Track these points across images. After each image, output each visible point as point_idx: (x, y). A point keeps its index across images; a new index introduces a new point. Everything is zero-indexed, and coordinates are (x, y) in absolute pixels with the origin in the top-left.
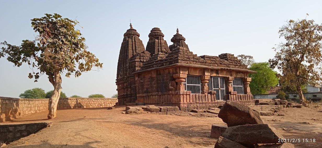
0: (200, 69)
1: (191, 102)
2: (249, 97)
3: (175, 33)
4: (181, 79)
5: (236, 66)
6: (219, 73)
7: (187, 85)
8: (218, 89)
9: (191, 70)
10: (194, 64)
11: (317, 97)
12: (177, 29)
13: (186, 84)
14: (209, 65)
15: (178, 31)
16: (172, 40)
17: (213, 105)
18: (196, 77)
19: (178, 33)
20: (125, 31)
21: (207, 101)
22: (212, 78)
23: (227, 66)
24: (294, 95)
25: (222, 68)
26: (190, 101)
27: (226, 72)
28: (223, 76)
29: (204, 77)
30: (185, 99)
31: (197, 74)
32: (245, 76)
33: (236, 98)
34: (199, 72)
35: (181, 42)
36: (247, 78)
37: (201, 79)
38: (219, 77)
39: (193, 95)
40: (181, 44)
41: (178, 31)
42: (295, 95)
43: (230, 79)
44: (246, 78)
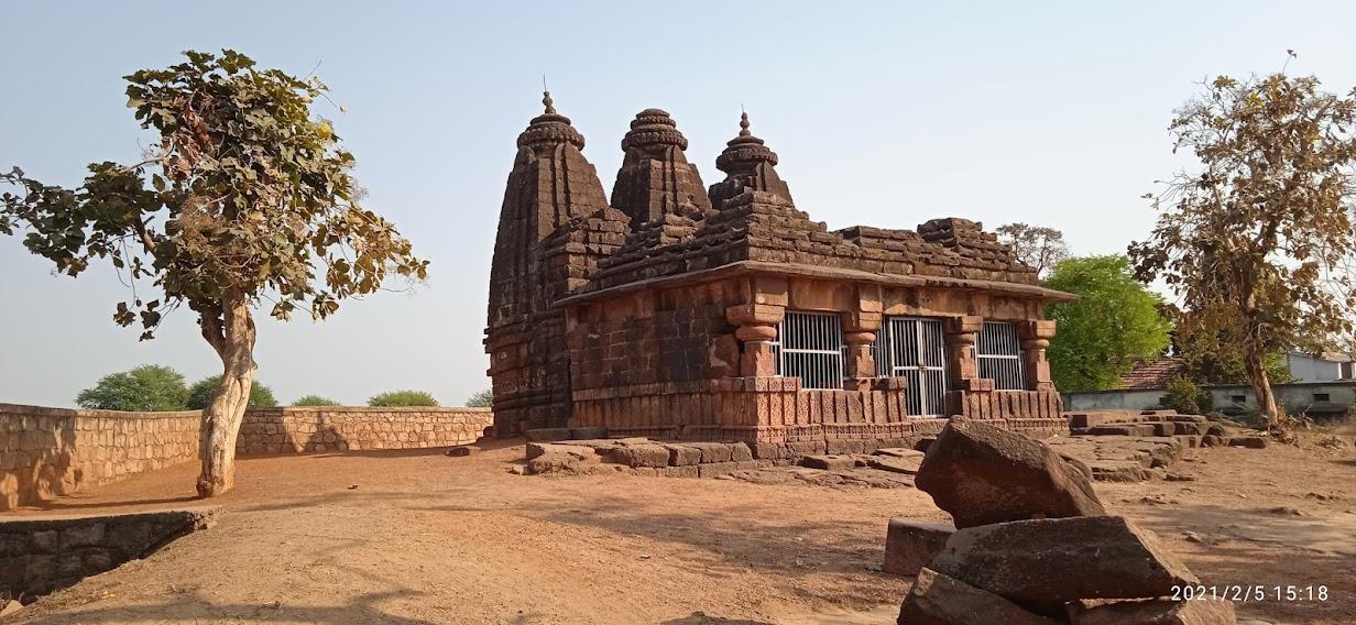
0: (839, 285)
1: (803, 422)
2: (1044, 405)
3: (734, 133)
6: (920, 302)
7: (786, 350)
8: (916, 368)
10: (813, 262)
11: (1333, 400)
12: (744, 117)
13: (778, 347)
15: (744, 125)
16: (722, 163)
17: (894, 435)
18: (821, 317)
19: (749, 133)
20: (714, 183)
21: (868, 420)
22: (891, 323)
23: (952, 272)
24: (1233, 393)
25: (931, 278)
26: (796, 422)
27: (949, 300)
28: (935, 313)
30: (776, 411)
31: (827, 304)
35: (758, 168)
36: (1039, 323)
37: (844, 327)
38: (921, 316)
39: (809, 394)
40: (758, 178)
41: (744, 125)
43: (965, 327)
44: (1034, 323)
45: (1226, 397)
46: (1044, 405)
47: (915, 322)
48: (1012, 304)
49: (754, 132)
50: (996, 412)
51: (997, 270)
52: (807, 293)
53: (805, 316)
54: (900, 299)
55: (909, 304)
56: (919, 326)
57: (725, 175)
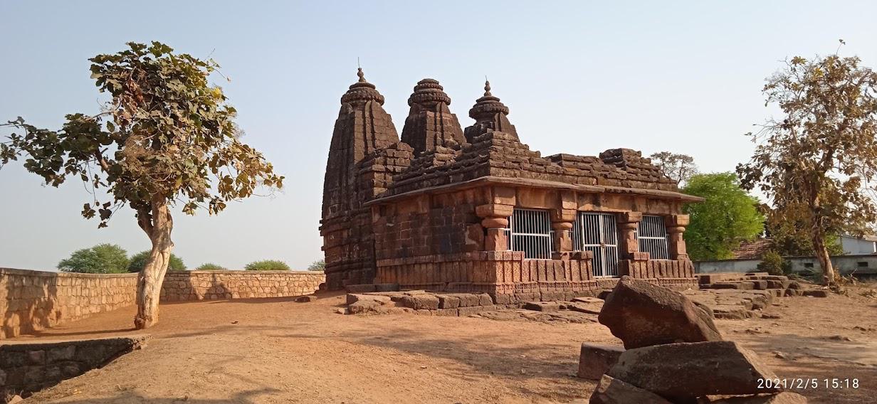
2: (682, 269)
3: (481, 94)
4: (496, 219)
5: (647, 182)
6: (601, 203)
7: (514, 234)
8: (598, 245)
9: (523, 195)
10: (532, 177)
11: (870, 266)
12: (487, 83)
14: (573, 180)
15: (487, 89)
16: (473, 113)
17: (585, 289)
23: (622, 183)
24: (805, 261)
27: (620, 199)
28: (611, 210)
29: (561, 214)
30: (508, 273)
31: (541, 204)
32: (670, 212)
33: (647, 269)
34: (545, 198)
35: (496, 117)
36: (678, 216)
37: (552, 219)
39: (530, 262)
40: (496, 123)
41: (487, 89)
42: (809, 261)
43: (630, 219)
44: (676, 217)
45: (801, 264)
46: (682, 269)
47: (598, 216)
48: (661, 204)
49: (493, 93)
50: (651, 274)
51: (650, 182)
52: (528, 197)
53: (533, 212)
54: (588, 201)
55: (594, 204)
56: (601, 218)
57: (475, 121)
